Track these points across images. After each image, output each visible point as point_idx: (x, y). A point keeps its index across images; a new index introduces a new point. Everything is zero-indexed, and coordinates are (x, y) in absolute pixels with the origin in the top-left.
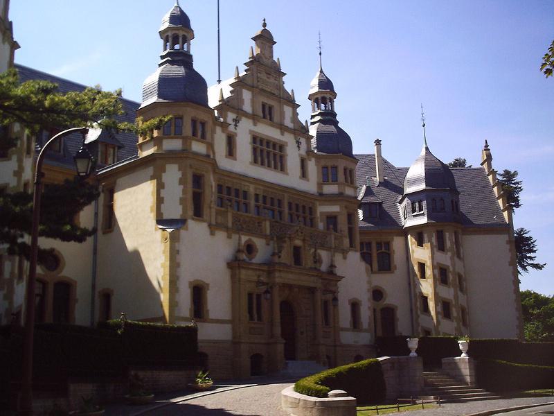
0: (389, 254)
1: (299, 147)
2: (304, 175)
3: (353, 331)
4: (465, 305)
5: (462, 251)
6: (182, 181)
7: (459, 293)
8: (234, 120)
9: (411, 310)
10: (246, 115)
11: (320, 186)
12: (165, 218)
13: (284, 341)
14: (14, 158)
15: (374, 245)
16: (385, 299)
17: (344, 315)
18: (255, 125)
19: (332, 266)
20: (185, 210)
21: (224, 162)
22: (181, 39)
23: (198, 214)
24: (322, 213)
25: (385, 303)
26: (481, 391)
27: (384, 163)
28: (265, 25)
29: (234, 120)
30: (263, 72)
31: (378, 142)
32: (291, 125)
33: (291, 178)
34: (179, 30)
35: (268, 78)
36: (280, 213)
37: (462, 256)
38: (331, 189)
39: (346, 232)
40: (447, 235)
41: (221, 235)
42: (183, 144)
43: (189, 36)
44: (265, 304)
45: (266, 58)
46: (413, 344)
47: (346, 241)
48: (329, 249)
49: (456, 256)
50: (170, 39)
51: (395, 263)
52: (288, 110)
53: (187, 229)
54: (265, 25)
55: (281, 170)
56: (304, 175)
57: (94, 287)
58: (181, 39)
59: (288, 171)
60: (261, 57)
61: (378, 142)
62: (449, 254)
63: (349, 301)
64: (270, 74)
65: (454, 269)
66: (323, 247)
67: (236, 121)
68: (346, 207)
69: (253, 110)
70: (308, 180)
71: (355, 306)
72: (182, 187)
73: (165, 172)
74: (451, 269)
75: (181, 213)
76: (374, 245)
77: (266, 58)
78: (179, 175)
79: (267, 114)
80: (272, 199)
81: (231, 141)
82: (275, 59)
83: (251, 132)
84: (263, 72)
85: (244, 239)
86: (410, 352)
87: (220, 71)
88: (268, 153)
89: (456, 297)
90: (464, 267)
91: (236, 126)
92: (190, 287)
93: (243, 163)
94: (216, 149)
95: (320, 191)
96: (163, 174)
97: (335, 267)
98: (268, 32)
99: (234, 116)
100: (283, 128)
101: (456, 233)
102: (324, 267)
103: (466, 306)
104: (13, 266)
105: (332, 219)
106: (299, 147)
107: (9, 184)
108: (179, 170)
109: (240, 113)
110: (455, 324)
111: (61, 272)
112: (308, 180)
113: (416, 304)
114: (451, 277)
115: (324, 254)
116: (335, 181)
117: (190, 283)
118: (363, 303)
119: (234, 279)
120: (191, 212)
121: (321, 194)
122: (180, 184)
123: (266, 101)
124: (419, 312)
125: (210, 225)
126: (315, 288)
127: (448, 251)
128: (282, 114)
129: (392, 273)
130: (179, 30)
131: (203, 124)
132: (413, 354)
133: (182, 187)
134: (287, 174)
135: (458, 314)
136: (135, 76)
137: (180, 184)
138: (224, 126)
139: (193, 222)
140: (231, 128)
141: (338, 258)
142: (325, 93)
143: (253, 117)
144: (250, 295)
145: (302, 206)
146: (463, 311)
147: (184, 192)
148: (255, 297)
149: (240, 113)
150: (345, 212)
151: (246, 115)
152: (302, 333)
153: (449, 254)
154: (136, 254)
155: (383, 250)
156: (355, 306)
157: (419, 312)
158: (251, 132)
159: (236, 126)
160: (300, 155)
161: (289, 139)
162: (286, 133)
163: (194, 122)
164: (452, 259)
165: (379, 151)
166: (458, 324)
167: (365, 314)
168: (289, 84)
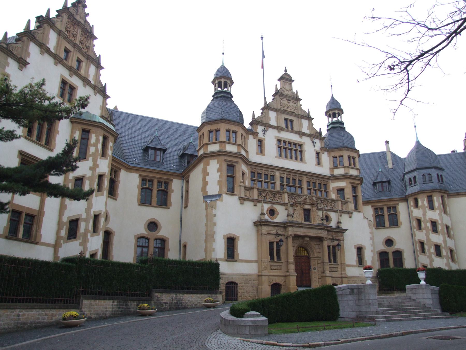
0: (396, 215)
1: (314, 145)
2: (319, 163)
3: (359, 267)
4: (453, 247)
5: (448, 208)
6: (219, 170)
7: (448, 239)
8: (262, 130)
9: (414, 252)
10: (272, 127)
11: (332, 169)
12: (209, 194)
13: (296, 274)
14: (90, 159)
15: (385, 209)
16: (395, 246)
17: (350, 256)
18: (301, 138)
19: (339, 222)
20: (221, 188)
21: (254, 157)
22: (337, 115)
23: (231, 191)
24: (333, 188)
25: (385, 248)
26: (257, 316)
27: (393, 155)
28: (286, 71)
29: (262, 130)
30: (285, 102)
31: (387, 142)
32: (307, 132)
33: (309, 165)
34: (223, 79)
35: (289, 103)
36: (274, 184)
37: (448, 212)
38: (339, 172)
39: (351, 199)
40: (435, 198)
41: (248, 205)
42: (220, 146)
43: (341, 113)
44: (283, 248)
45: (287, 91)
46: (422, 275)
47: (351, 206)
48: (336, 211)
49: (443, 212)
50: (332, 116)
51: (401, 221)
52: (305, 123)
53: (222, 201)
54: (286, 71)
55: (301, 160)
56: (319, 163)
57: (180, 241)
58: (337, 115)
59: (306, 161)
60: (283, 90)
61: (387, 142)
62: (438, 212)
63: (355, 246)
64: (290, 100)
65: (442, 221)
66: (332, 210)
67: (264, 131)
68: (351, 183)
69: (277, 123)
70: (322, 167)
71: (360, 250)
72: (219, 173)
73: (209, 165)
74: (440, 222)
75: (218, 190)
76: (385, 209)
77: (287, 91)
78: (218, 166)
79: (289, 125)
80: (293, 178)
81: (260, 143)
82: (294, 90)
83: (275, 137)
84: (285, 102)
85: (266, 207)
86: (420, 281)
87: (249, 101)
88: (288, 149)
89: (445, 241)
90: (451, 220)
91: (264, 134)
92: (224, 239)
93: (271, 157)
94: (249, 149)
95: (332, 173)
96: (208, 167)
97: (341, 223)
98: (289, 75)
99: (263, 128)
100: (301, 134)
101: (442, 197)
102: (333, 224)
103: (454, 248)
104: (87, 226)
105: (341, 191)
106: (314, 145)
107: (86, 175)
108: (218, 163)
109: (268, 126)
110: (445, 261)
111: (158, 232)
112: (322, 167)
113: (416, 248)
114: (440, 228)
115: (333, 215)
116: (342, 166)
117: (224, 236)
118: (366, 247)
119: (260, 234)
120: (225, 190)
121: (333, 175)
122: (218, 172)
123: (287, 117)
124: (419, 253)
125: (240, 199)
126: (323, 237)
127: (436, 209)
128: (301, 125)
129: (399, 227)
130: (223, 79)
131: (354, 158)
132: (423, 282)
133: (219, 173)
134: (306, 163)
135: (447, 253)
136: (187, 107)
137: (218, 172)
138: (255, 134)
139: (227, 196)
140: (261, 136)
141: (345, 217)
142: (334, 109)
143: (279, 128)
144: (271, 243)
145: (319, 183)
146: (451, 251)
147: (221, 176)
148: (331, 247)
149: (268, 126)
150: (350, 186)
151: (272, 127)
152: (315, 269)
153: (438, 212)
154: (66, 205)
155: (163, 188)
156: (360, 250)
157: (419, 253)
158: (275, 137)
159: (264, 134)
160: (315, 150)
161: (306, 141)
162: (304, 137)
163: (349, 157)
164: (440, 214)
165: (388, 148)
166: (448, 261)
167: (370, 257)
168: (305, 105)
